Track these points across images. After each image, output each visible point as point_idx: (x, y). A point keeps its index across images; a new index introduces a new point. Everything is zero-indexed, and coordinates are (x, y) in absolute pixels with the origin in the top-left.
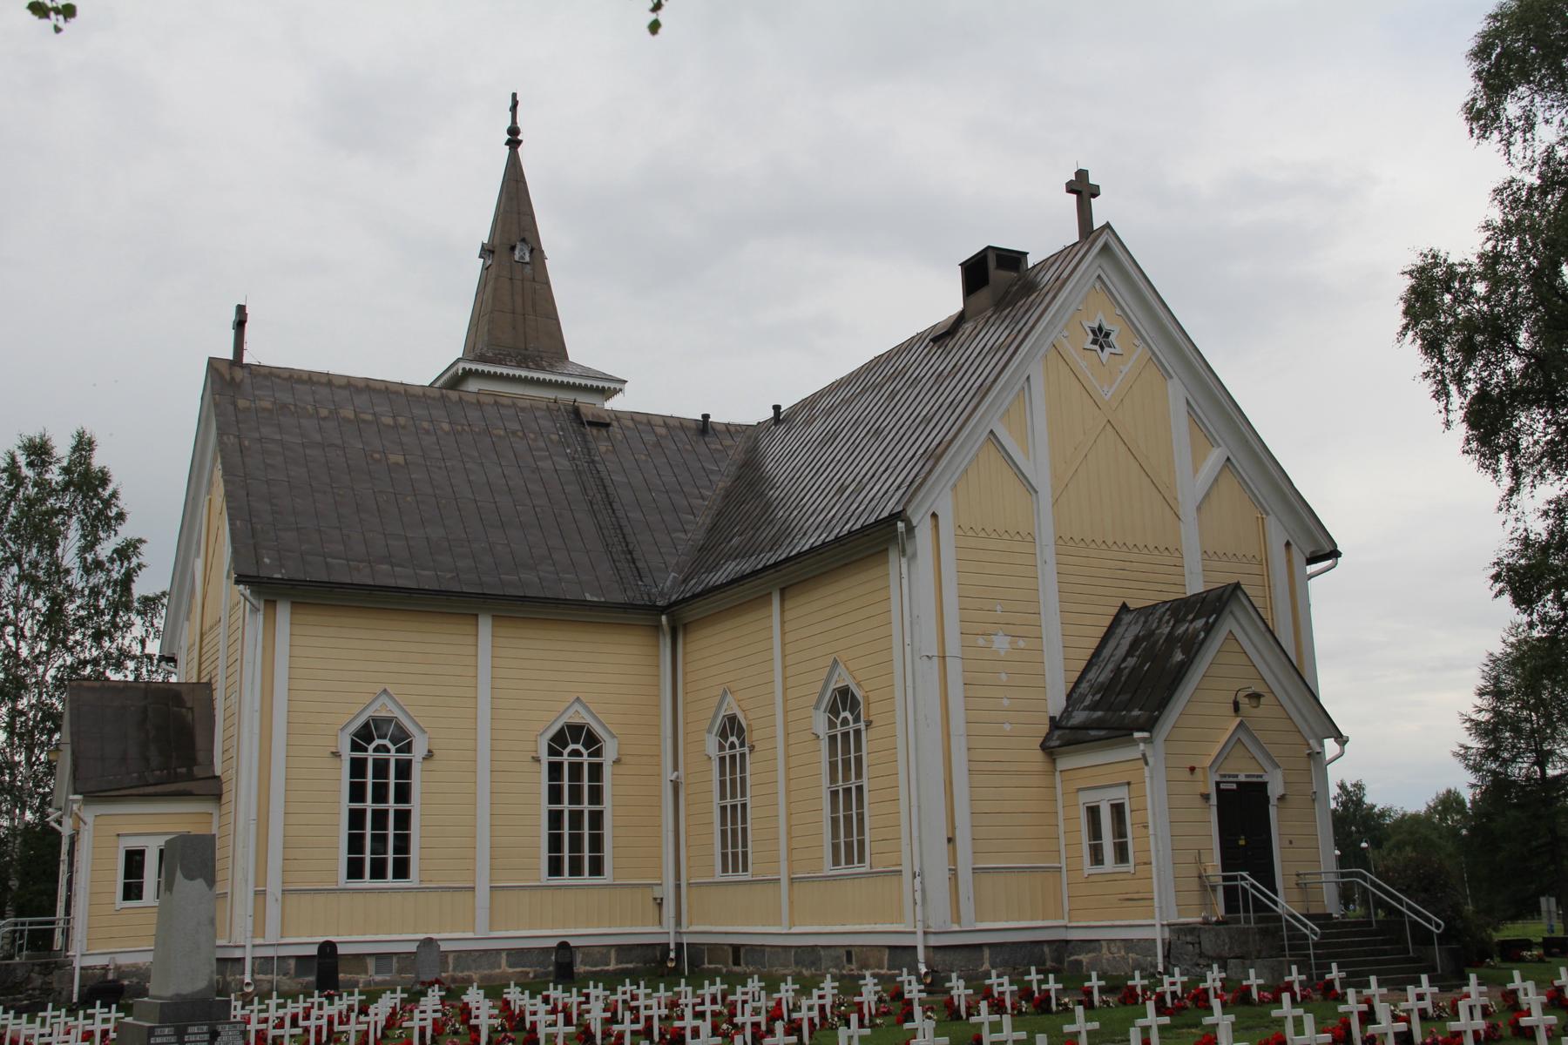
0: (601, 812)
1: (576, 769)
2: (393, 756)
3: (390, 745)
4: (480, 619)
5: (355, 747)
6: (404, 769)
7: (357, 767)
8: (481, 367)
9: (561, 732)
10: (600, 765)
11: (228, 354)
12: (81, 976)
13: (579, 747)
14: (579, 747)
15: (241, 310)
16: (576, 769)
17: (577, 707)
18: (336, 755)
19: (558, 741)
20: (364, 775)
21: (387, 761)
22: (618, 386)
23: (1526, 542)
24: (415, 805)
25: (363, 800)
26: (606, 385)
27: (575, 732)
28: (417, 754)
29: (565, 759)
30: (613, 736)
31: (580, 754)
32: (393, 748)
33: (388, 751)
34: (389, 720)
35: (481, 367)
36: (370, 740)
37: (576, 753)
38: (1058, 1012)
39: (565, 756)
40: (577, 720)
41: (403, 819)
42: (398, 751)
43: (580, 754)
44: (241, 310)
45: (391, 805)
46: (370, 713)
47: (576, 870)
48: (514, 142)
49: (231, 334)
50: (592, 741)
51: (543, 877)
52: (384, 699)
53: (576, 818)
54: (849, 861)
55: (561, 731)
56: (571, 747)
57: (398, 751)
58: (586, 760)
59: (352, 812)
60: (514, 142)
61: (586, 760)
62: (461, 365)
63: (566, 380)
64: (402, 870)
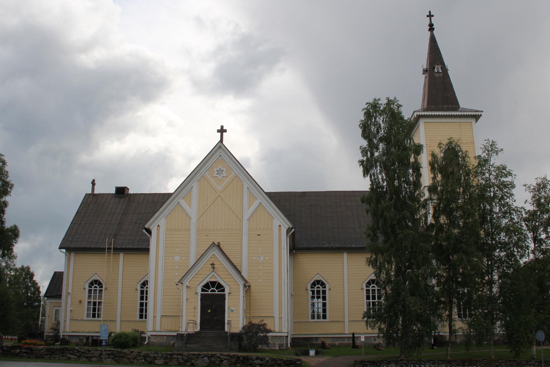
5: (142, 287)
6: (324, 292)
7: (368, 291)
8: (426, 113)
11: (224, 133)
13: (319, 286)
20: (372, 296)
22: (480, 113)
23: (421, 167)
25: (370, 299)
26: (477, 113)
27: (96, 282)
28: (103, 289)
34: (97, 280)
35: (426, 113)
36: (93, 285)
37: (96, 287)
38: (105, 346)
40: (96, 279)
46: (315, 279)
47: (319, 317)
48: (431, 28)
50: (323, 284)
51: (310, 320)
55: (369, 281)
56: (317, 286)
58: (321, 289)
60: (431, 28)
61: (321, 289)
62: (415, 114)
63: (463, 113)
64: (324, 317)
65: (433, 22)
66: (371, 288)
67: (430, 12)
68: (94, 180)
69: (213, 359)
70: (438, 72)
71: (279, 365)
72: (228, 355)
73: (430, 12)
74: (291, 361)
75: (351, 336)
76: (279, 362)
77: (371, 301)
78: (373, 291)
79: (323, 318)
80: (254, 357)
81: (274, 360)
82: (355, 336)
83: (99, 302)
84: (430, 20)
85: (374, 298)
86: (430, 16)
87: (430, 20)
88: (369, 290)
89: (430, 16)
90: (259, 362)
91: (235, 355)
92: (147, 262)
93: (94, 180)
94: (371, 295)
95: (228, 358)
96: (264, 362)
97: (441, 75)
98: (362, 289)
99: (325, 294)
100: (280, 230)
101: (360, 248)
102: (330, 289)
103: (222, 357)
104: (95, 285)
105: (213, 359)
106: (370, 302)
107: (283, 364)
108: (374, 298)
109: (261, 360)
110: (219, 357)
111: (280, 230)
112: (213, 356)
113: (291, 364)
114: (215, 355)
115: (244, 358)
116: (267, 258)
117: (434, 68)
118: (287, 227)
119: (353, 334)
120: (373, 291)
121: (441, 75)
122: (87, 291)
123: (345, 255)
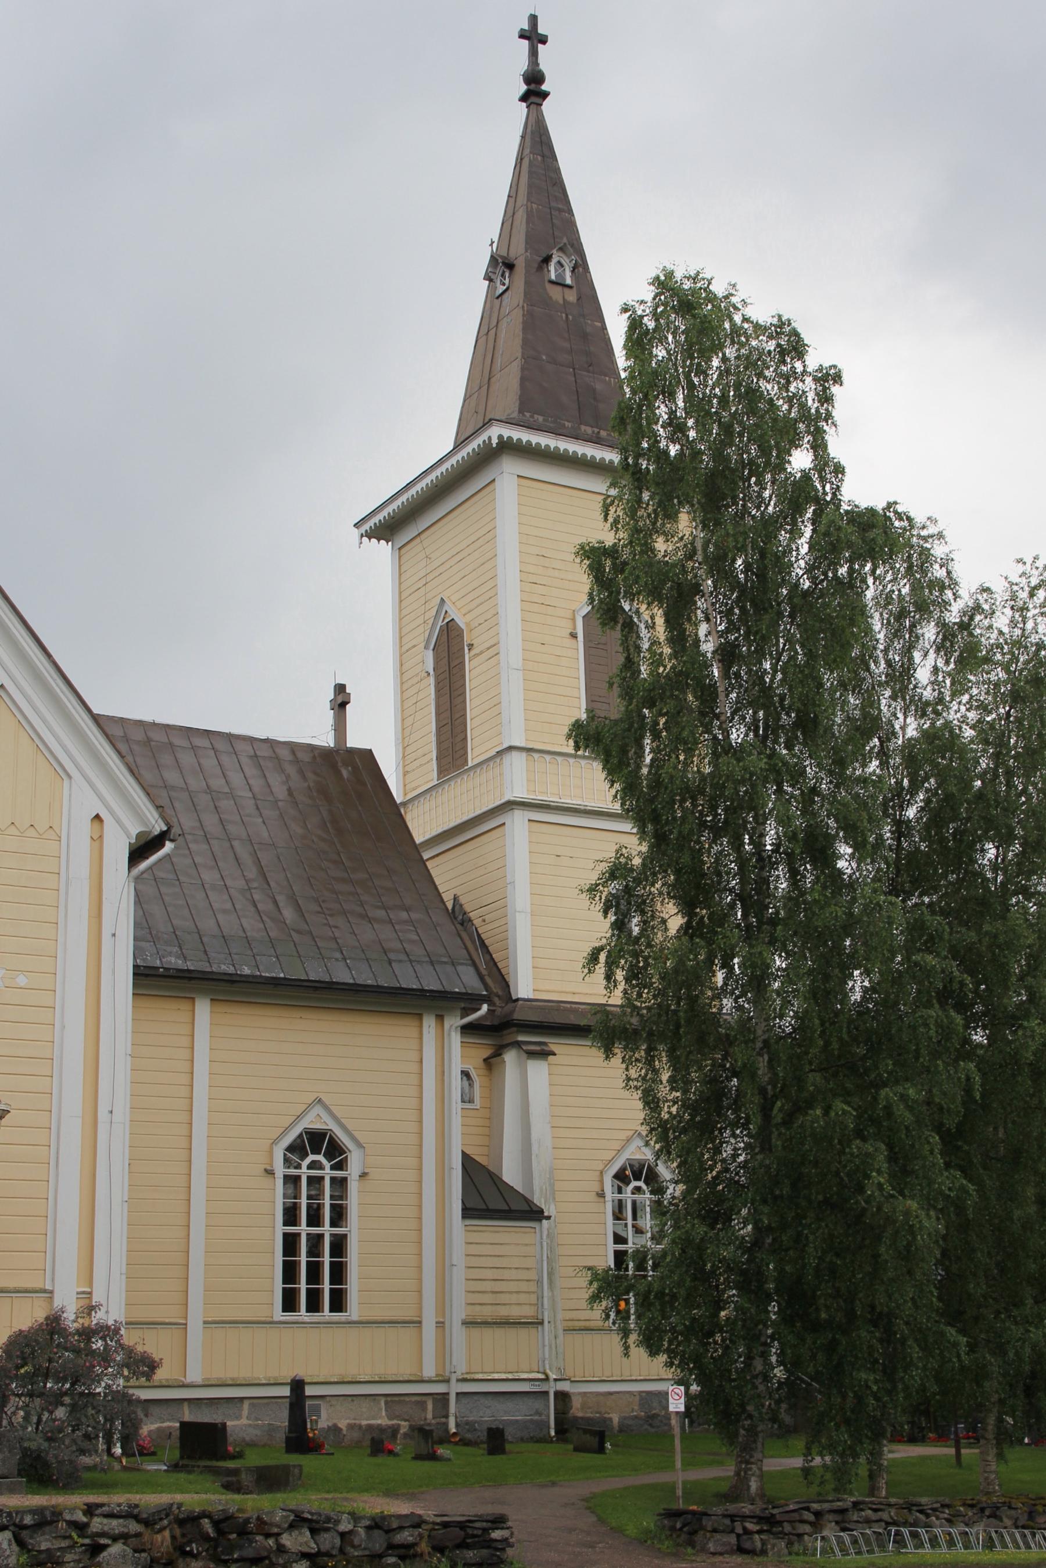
0: (344, 1237)
3: (644, 1187)
4: (197, 1001)
10: (344, 1180)
14: (320, 1158)
15: (340, 689)
17: (318, 1110)
19: (297, 1149)
24: (354, 1228)
27: (316, 1141)
29: (304, 1172)
30: (359, 1145)
31: (321, 1167)
32: (327, 1164)
37: (638, 1189)
39: (304, 1169)
40: (318, 1126)
41: (339, 1246)
42: (332, 1168)
43: (321, 1167)
44: (340, 689)
45: (326, 1229)
47: (314, 1305)
48: (534, 91)
49: (329, 716)
50: (335, 1151)
51: (278, 1314)
53: (315, 1242)
54: (314, 1305)
57: (332, 1168)
59: (286, 1235)
60: (534, 91)
64: (338, 1303)
65: (543, 66)
66: (304, 1172)
67: (533, 19)
69: (44, 1543)
70: (559, 284)
71: (406, 1552)
72: (131, 1514)
73: (533, 19)
74: (462, 1525)
75: (286, 1391)
76: (406, 1536)
77: (303, 1229)
78: (315, 1182)
80: (278, 1516)
81: (378, 1524)
82: (309, 1391)
83: (311, 1180)
84: (534, 54)
85: (315, 1219)
86: (533, 36)
87: (534, 54)
90: (296, 1541)
91: (166, 1511)
92: (145, 931)
94: (304, 1202)
95: (134, 1527)
96: (329, 1541)
97: (571, 296)
98: (270, 1173)
100: (98, 840)
101: (275, 983)
102: (363, 1175)
103: (97, 1524)
105: (44, 1543)
107: (424, 1547)
108: (315, 1219)
109: (314, 1532)
110: (81, 1528)
111: (98, 840)
112: (46, 1520)
113: (462, 1545)
114: (57, 1514)
115: (223, 1522)
116: (22, 980)
117: (547, 260)
118: (135, 830)
119: (298, 1386)
120: (315, 1182)
121: (571, 296)
123: (203, 1008)
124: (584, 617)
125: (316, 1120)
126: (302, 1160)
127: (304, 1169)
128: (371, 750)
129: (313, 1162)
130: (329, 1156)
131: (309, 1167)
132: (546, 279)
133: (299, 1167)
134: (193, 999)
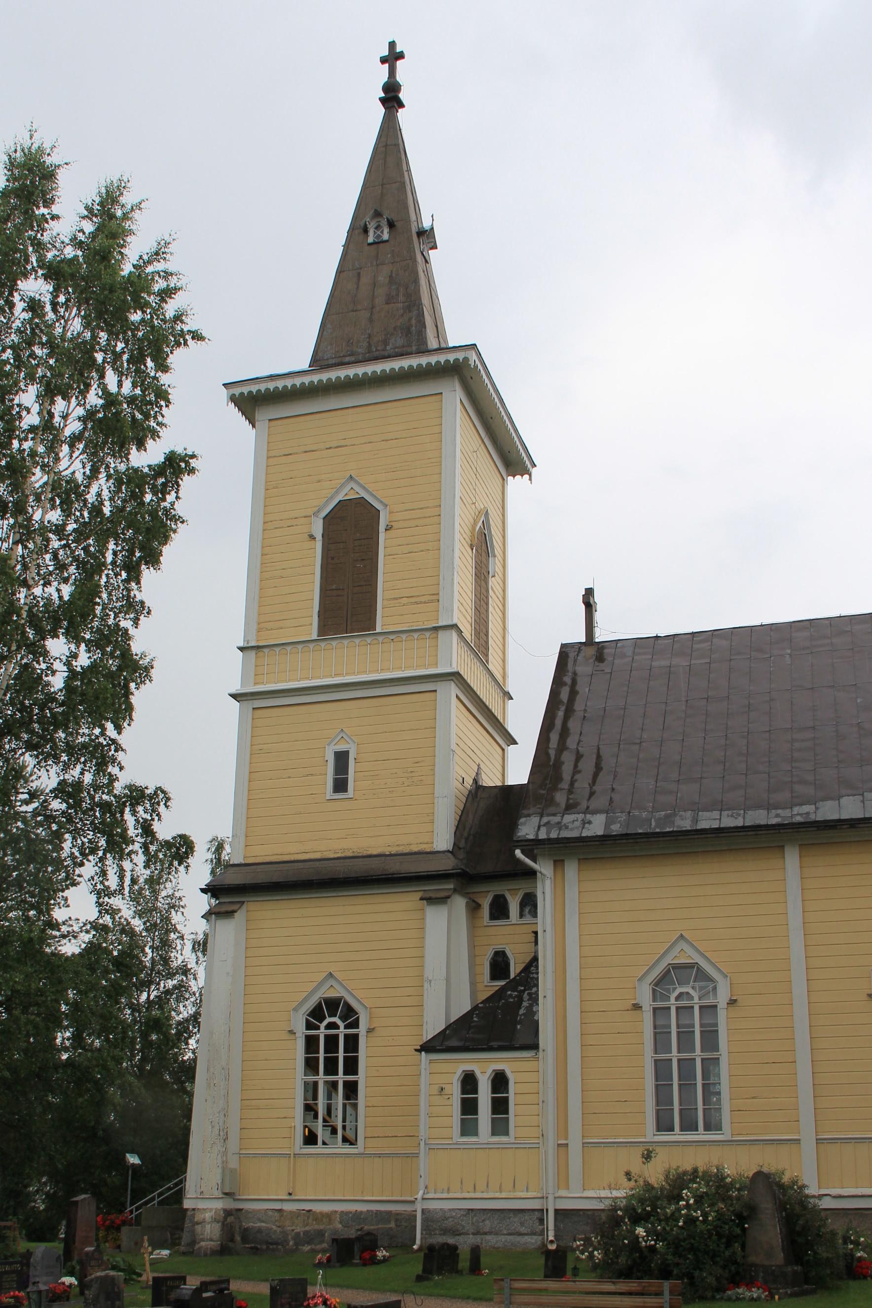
1: (331, 1041)
2: (342, 1032)
4: (787, 849)
5: (309, 1026)
6: (352, 1042)
7: (311, 1043)
9: (666, 974)
10: (356, 1037)
12: (424, 1221)
13: (336, 1019)
14: (336, 1019)
16: (331, 1041)
18: (637, 1007)
19: (317, 1014)
21: (336, 1037)
27: (332, 1005)
28: (362, 1030)
32: (341, 1025)
33: (338, 1027)
36: (321, 1019)
39: (673, 1001)
42: (346, 1027)
45: (341, 1077)
47: (689, 1125)
48: (391, 98)
50: (350, 1015)
51: (457, 1137)
52: (682, 945)
56: (329, 1020)
57: (346, 1027)
60: (391, 98)
61: (342, 1032)
65: (400, 78)
66: (322, 1032)
67: (392, 45)
68: (589, 592)
73: (392, 45)
77: (322, 1078)
79: (708, 1128)
84: (392, 72)
87: (392, 72)
88: (317, 1038)
89: (393, 57)
93: (589, 592)
99: (356, 1050)
102: (732, 1002)
104: (329, 1020)
106: (316, 1084)
122: (301, 1044)
124: (324, 518)
125: (685, 955)
126: (321, 1023)
127: (673, 1001)
128: (563, 646)
129: (681, 994)
130: (343, 1018)
131: (677, 999)
132: (414, 230)
133: (318, 1028)
134: (783, 846)
